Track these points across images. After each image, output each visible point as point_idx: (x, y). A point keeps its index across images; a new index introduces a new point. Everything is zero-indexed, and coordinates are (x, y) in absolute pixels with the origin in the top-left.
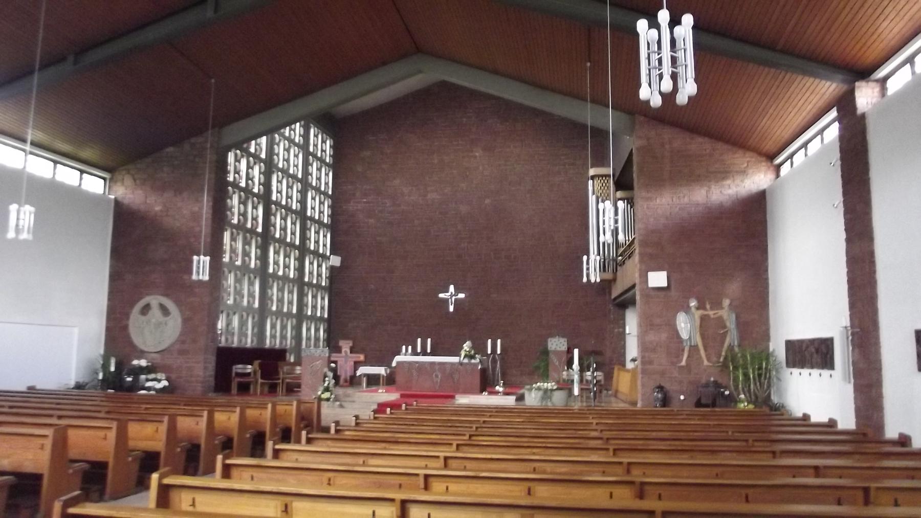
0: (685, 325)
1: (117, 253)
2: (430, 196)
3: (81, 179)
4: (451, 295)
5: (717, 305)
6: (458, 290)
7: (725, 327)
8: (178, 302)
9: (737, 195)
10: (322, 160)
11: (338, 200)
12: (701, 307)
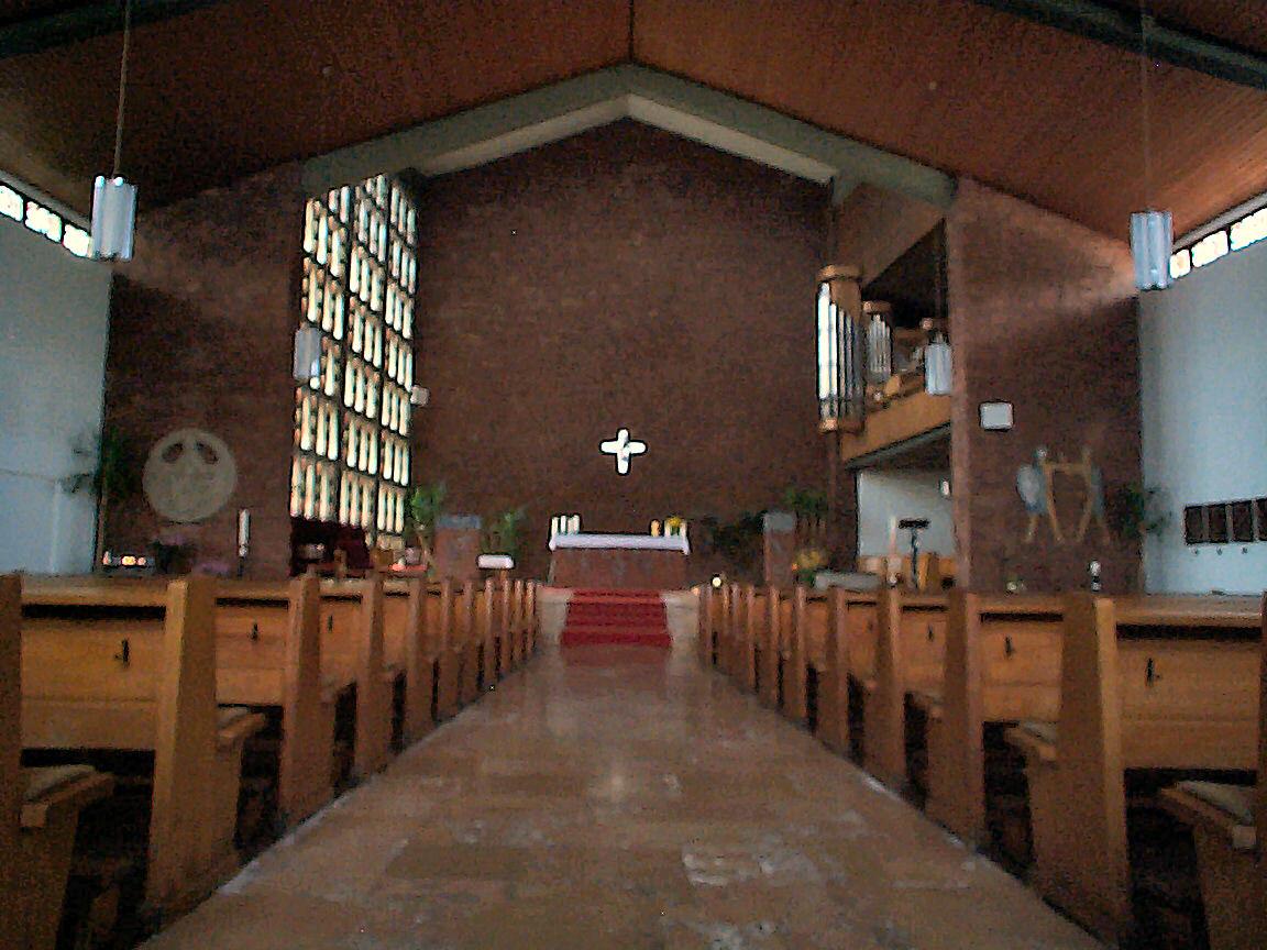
0: (1030, 485)
1: (116, 360)
2: (565, 303)
3: (63, 232)
4: (622, 449)
5: (1074, 457)
6: (630, 439)
7: (1084, 488)
8: (227, 439)
9: (1100, 301)
10: (403, 238)
11: (422, 301)
12: (1052, 458)
